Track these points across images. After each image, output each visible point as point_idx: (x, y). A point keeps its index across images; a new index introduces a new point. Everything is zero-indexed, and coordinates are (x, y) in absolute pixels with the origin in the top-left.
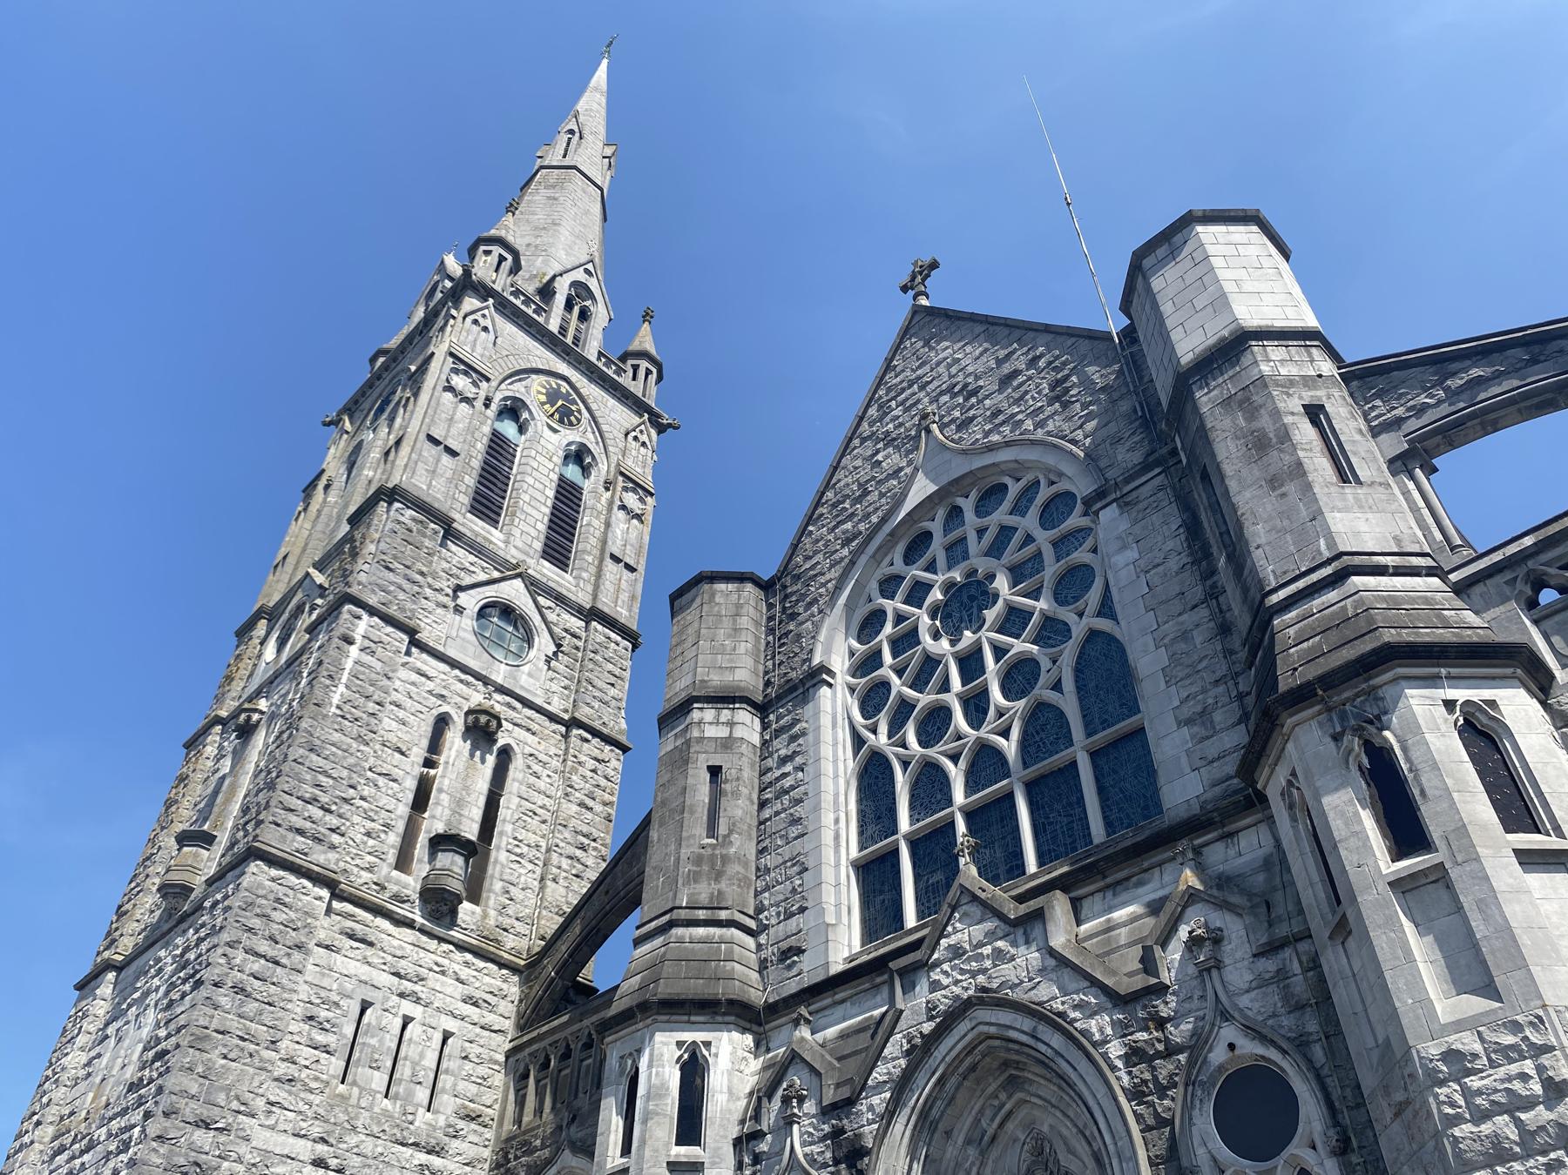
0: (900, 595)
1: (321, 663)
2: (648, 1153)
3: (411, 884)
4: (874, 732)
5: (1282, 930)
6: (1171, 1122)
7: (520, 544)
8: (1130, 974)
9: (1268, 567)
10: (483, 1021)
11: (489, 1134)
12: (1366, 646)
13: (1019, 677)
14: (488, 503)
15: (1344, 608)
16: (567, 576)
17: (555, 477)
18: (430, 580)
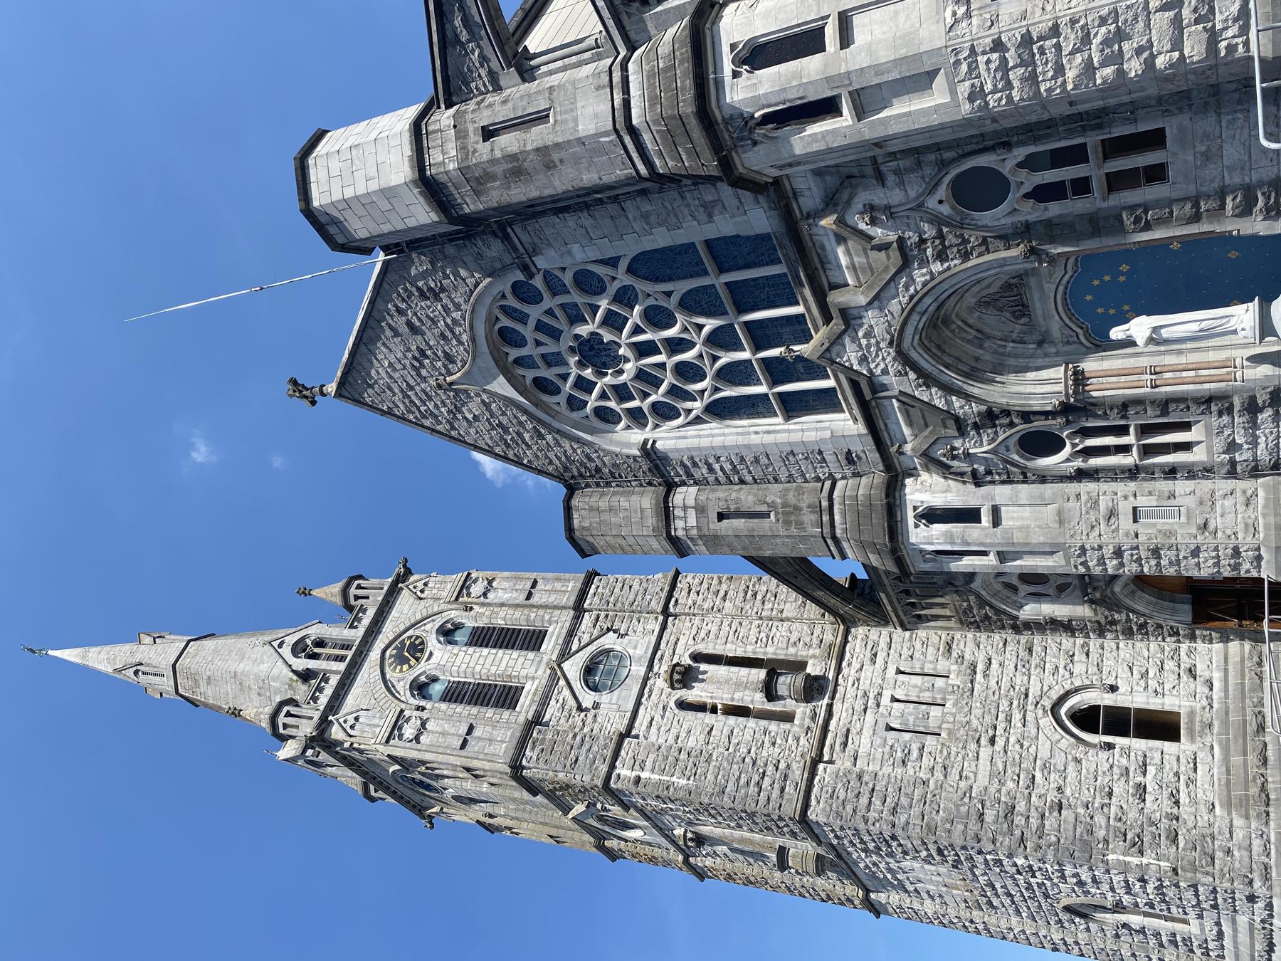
0: (584, 397)
1: (658, 797)
2: (988, 541)
4: (690, 411)
5: (869, 170)
6: (985, 238)
7: (533, 669)
8: (889, 258)
9: (621, 173)
10: (886, 649)
11: (958, 635)
12: (693, 124)
13: (657, 317)
14: (506, 697)
15: (658, 131)
16: (550, 630)
17: (471, 650)
18: (577, 730)
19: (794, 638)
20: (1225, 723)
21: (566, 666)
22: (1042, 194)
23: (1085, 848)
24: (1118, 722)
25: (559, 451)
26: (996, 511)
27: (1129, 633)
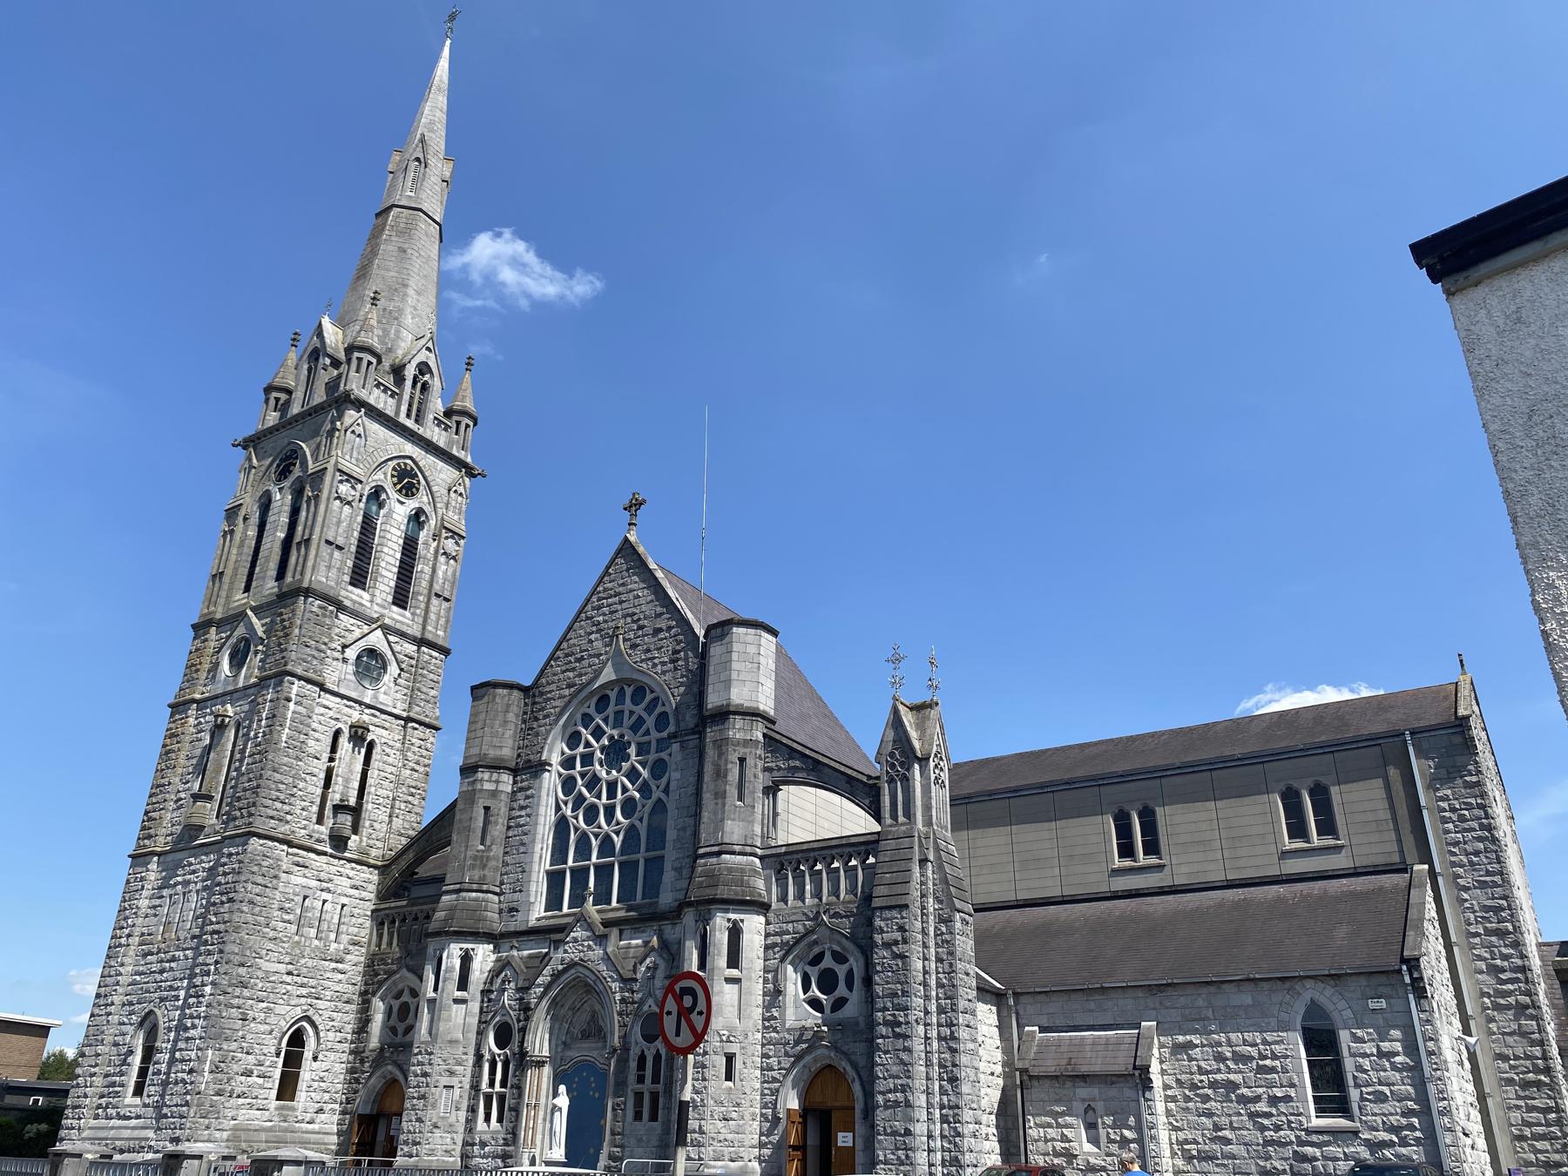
3: (324, 830)
4: (566, 803)
14: (359, 577)
16: (407, 614)
19: (376, 825)
20: (286, 1130)
21: (379, 632)
22: (642, 1059)
23: (214, 1034)
24: (293, 1060)
25: (557, 694)
26: (463, 1001)
27: (351, 1071)
